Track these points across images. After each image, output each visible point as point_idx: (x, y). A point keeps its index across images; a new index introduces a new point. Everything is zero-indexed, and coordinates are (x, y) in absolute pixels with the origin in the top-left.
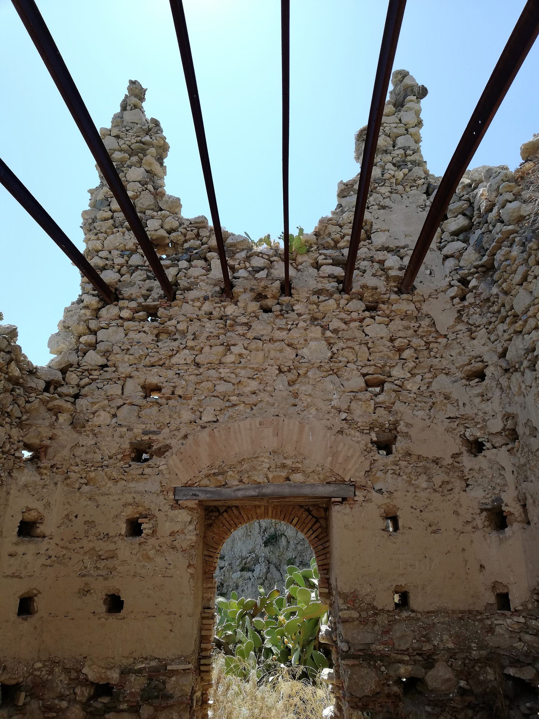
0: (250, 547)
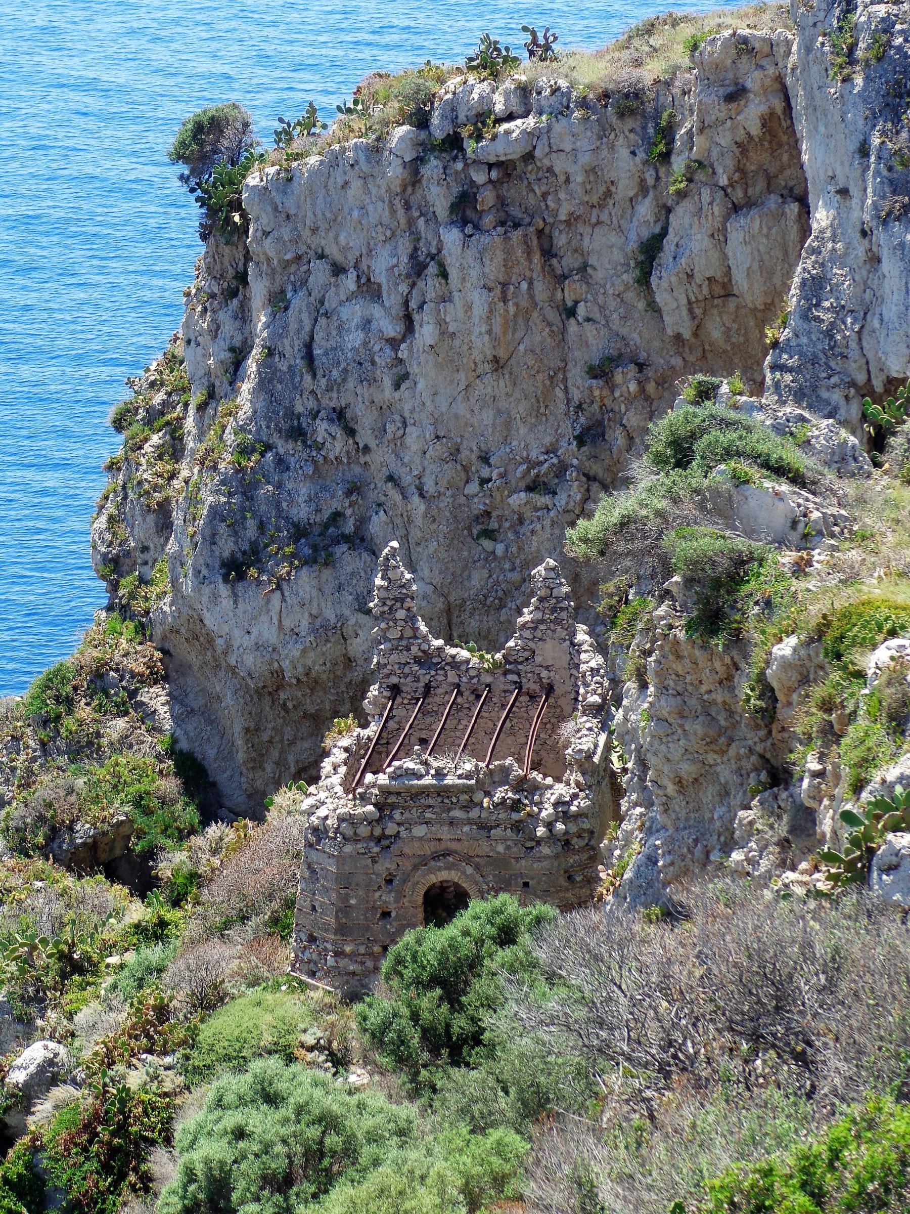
0: (547, 440)
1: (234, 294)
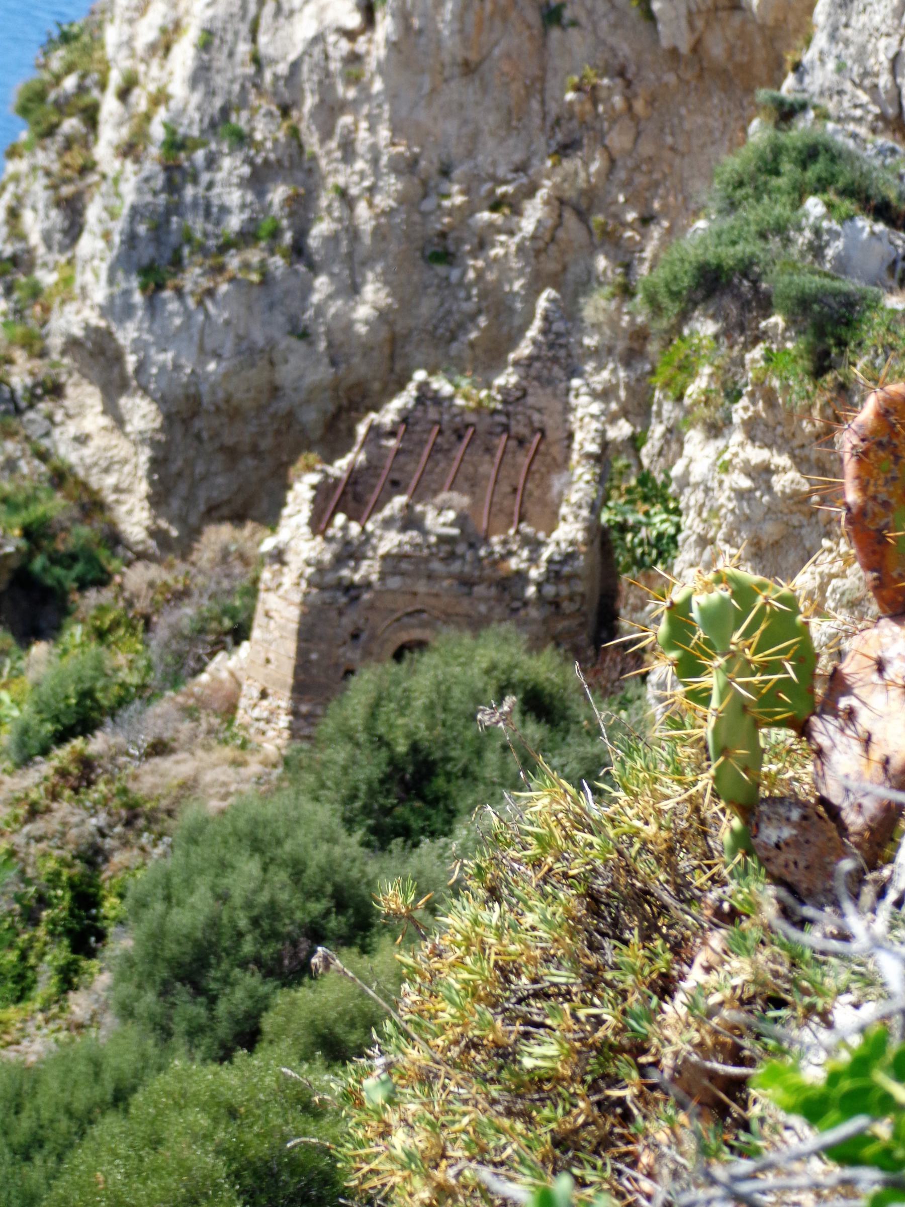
0: (518, 157)
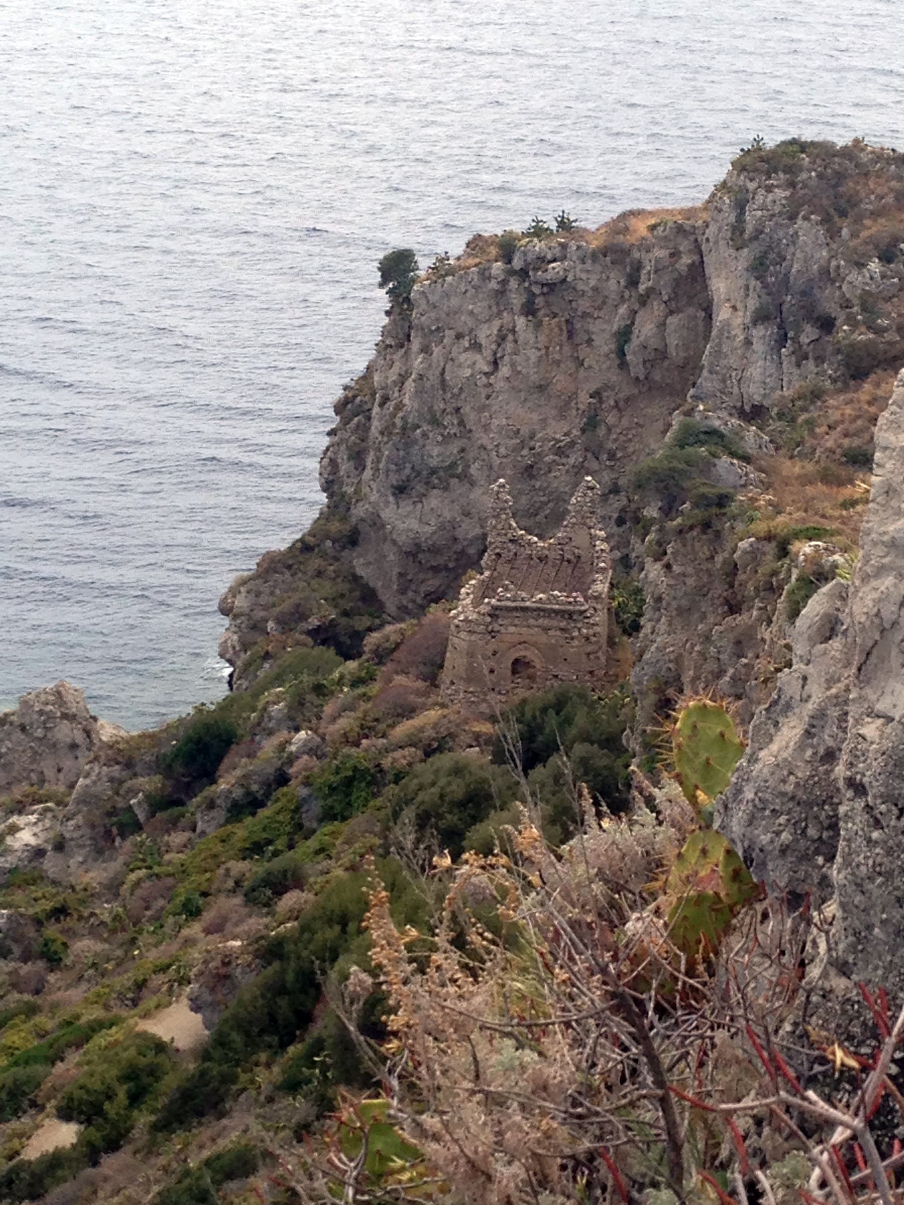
1: (402, 346)
